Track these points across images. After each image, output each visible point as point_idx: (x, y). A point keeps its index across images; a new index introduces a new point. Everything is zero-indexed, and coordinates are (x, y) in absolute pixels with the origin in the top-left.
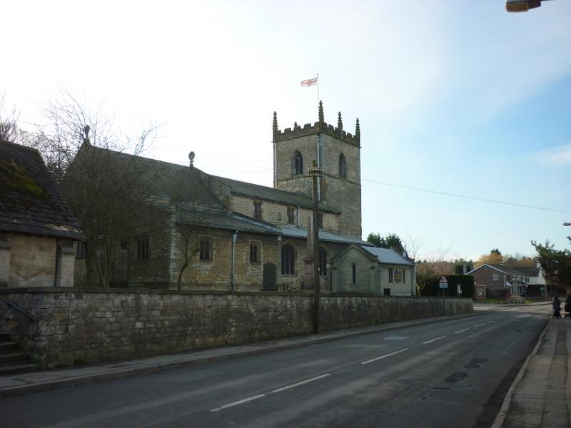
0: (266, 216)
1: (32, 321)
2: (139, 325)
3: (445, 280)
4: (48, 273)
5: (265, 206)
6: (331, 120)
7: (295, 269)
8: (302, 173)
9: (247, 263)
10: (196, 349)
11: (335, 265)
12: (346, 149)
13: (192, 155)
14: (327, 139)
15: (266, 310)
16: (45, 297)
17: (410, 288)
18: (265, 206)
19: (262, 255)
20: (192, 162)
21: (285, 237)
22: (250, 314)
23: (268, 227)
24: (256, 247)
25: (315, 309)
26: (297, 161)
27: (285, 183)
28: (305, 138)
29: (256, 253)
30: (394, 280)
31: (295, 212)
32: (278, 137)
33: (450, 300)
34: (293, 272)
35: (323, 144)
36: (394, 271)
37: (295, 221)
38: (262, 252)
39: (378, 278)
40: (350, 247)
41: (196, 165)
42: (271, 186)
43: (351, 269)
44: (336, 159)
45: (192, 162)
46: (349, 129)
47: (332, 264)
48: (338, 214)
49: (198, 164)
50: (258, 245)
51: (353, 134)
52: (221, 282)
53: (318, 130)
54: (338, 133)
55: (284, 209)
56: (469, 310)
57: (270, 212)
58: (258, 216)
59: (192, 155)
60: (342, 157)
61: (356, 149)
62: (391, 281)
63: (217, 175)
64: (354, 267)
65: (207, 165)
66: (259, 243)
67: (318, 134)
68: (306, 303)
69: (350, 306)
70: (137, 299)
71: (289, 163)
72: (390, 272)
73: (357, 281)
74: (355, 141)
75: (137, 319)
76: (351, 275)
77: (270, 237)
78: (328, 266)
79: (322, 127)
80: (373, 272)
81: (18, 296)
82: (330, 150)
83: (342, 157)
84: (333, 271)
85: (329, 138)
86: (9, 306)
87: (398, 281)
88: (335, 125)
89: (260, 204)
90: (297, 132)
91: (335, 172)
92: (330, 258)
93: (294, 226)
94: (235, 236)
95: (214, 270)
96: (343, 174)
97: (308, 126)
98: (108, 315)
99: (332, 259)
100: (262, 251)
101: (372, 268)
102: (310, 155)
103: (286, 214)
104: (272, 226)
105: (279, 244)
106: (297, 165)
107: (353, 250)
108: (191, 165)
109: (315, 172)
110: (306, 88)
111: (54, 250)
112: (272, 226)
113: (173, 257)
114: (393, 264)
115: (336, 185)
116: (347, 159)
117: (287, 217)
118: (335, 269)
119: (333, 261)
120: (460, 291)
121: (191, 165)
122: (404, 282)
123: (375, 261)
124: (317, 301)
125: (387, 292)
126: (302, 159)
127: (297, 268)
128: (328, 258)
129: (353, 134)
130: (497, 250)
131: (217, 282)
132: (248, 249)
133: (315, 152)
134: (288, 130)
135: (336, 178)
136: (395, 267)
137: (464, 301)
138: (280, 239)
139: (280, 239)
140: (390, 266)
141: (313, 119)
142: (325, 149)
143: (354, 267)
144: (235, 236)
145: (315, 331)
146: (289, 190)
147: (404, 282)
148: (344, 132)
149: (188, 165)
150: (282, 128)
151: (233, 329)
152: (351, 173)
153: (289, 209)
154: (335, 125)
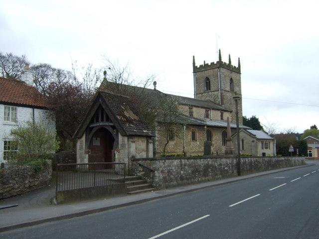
0: (195, 115)
1: (152, 171)
2: (182, 172)
3: (292, 147)
4: (145, 151)
6: (225, 60)
8: (210, 89)
10: (199, 182)
12: (234, 75)
13: (155, 83)
14: (223, 70)
15: (221, 165)
17: (272, 152)
18: (194, 109)
20: (155, 87)
21: (208, 126)
22: (216, 167)
23: (199, 121)
25: (238, 164)
26: (207, 83)
27: (200, 95)
29: (194, 135)
31: (209, 112)
32: (196, 70)
33: (294, 158)
35: (221, 73)
36: (264, 143)
37: (209, 117)
38: (197, 134)
39: (256, 147)
41: (157, 88)
42: (193, 98)
44: (229, 81)
45: (155, 87)
46: (235, 64)
48: (231, 112)
49: (159, 88)
51: (237, 66)
53: (218, 65)
54: (229, 67)
55: (204, 110)
56: (303, 163)
57: (199, 113)
58: (191, 114)
59: (155, 83)
60: (231, 80)
62: (263, 148)
65: (163, 88)
67: (218, 68)
68: (235, 161)
69: (251, 162)
70: (181, 162)
71: (203, 84)
72: (262, 144)
74: (237, 70)
75: (181, 170)
77: (201, 126)
79: (220, 64)
80: (253, 144)
81: (143, 162)
82: (225, 76)
83: (231, 80)
85: (225, 70)
86: (140, 165)
87: (266, 148)
88: (227, 62)
90: (205, 67)
91: (228, 88)
94: (185, 127)
95: (176, 144)
97: (212, 64)
98: (173, 168)
100: (197, 134)
101: (253, 141)
104: (201, 121)
105: (206, 130)
106: (207, 85)
108: (155, 89)
109: (236, 97)
111: (146, 142)
112: (201, 121)
113: (157, 139)
114: (265, 139)
115: (229, 96)
116: (234, 81)
120: (55, 202)
121: (155, 89)
123: (254, 138)
124: (239, 160)
125: (264, 154)
126: (210, 82)
129: (237, 66)
130: (315, 125)
132: (191, 133)
134: (201, 66)
136: (265, 141)
137: (300, 158)
138: (205, 127)
139: (205, 127)
141: (215, 60)
142: (222, 76)
144: (185, 127)
145: (239, 174)
146: (203, 99)
148: (232, 66)
149: (153, 88)
150: (198, 65)
151: (210, 174)
152: (236, 89)
153: (206, 110)
154: (227, 62)
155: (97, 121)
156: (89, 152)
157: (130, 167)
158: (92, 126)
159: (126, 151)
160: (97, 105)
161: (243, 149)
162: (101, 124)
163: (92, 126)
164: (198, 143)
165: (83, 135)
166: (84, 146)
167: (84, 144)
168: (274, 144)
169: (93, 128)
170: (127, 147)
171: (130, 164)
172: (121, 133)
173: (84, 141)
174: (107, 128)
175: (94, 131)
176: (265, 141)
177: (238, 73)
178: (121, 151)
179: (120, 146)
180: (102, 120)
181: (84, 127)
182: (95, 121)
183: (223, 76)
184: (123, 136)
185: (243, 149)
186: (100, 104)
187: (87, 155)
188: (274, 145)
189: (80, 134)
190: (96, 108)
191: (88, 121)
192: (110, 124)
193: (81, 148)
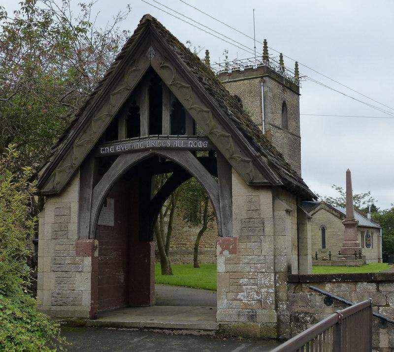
6: (275, 64)
12: (288, 96)
17: (376, 254)
28: (246, 82)
36: (365, 234)
40: (319, 207)
44: (280, 107)
46: (290, 74)
52: (209, 249)
60: (284, 105)
61: (296, 96)
64: (323, 229)
74: (293, 88)
76: (320, 240)
82: (274, 96)
85: (274, 82)
96: (285, 127)
102: (252, 102)
107: (323, 211)
110: (127, 6)
131: (206, 249)
133: (258, 98)
135: (279, 128)
142: (270, 94)
143: (323, 229)
152: (291, 124)
155: (133, 132)
156: (94, 248)
157: (118, 307)
158: (110, 149)
159: (267, 246)
160: (142, 67)
161: (324, 247)
162: (153, 142)
163: (110, 149)
165: (68, 184)
166: (73, 227)
167: (74, 218)
168: (378, 237)
169: (113, 158)
170: (269, 228)
171: (283, 294)
172: (240, 175)
173: (75, 206)
174: (176, 158)
175: (118, 168)
176: (366, 230)
177: (296, 93)
178: (242, 246)
179: (235, 229)
180: (155, 128)
181: (78, 155)
182: (123, 132)
183: (270, 94)
184: (254, 186)
185: (324, 247)
186: (150, 71)
187: (88, 261)
188: (379, 239)
189: (59, 178)
190: (132, 80)
191: (98, 128)
192: (191, 143)
193: (60, 232)
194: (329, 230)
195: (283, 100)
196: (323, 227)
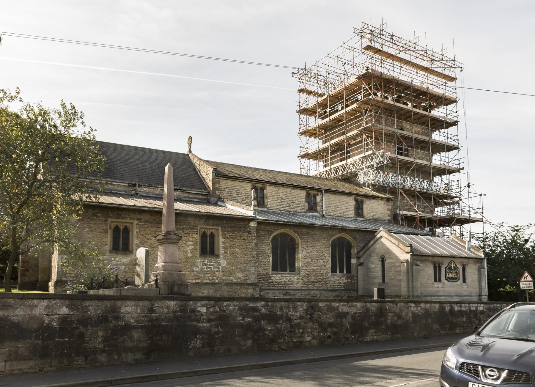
5: (269, 191)
7: (297, 265)
9: (194, 257)
11: (362, 260)
16: (116, 302)
19: (221, 245)
24: (212, 236)
30: (443, 278)
31: (318, 198)
34: (293, 269)
37: (318, 208)
43: (380, 263)
47: (358, 258)
50: (215, 232)
63: (130, 145)
64: (383, 261)
66: (218, 229)
73: (386, 280)
76: (380, 272)
78: (353, 261)
84: (359, 267)
89: (262, 189)
92: (356, 252)
93: (318, 214)
99: (359, 252)
100: (221, 240)
103: (304, 199)
117: (306, 204)
118: (361, 264)
119: (361, 254)
122: (464, 281)
127: (299, 264)
128: (354, 251)
132: (197, 237)
140: (436, 259)
143: (383, 261)
147: (464, 281)
161: (383, 280)
164: (223, 262)
194: (388, 261)
195: (364, 50)
196: (383, 258)
